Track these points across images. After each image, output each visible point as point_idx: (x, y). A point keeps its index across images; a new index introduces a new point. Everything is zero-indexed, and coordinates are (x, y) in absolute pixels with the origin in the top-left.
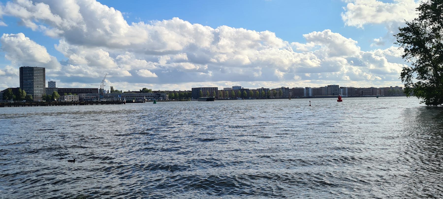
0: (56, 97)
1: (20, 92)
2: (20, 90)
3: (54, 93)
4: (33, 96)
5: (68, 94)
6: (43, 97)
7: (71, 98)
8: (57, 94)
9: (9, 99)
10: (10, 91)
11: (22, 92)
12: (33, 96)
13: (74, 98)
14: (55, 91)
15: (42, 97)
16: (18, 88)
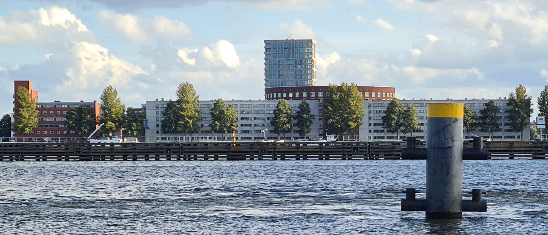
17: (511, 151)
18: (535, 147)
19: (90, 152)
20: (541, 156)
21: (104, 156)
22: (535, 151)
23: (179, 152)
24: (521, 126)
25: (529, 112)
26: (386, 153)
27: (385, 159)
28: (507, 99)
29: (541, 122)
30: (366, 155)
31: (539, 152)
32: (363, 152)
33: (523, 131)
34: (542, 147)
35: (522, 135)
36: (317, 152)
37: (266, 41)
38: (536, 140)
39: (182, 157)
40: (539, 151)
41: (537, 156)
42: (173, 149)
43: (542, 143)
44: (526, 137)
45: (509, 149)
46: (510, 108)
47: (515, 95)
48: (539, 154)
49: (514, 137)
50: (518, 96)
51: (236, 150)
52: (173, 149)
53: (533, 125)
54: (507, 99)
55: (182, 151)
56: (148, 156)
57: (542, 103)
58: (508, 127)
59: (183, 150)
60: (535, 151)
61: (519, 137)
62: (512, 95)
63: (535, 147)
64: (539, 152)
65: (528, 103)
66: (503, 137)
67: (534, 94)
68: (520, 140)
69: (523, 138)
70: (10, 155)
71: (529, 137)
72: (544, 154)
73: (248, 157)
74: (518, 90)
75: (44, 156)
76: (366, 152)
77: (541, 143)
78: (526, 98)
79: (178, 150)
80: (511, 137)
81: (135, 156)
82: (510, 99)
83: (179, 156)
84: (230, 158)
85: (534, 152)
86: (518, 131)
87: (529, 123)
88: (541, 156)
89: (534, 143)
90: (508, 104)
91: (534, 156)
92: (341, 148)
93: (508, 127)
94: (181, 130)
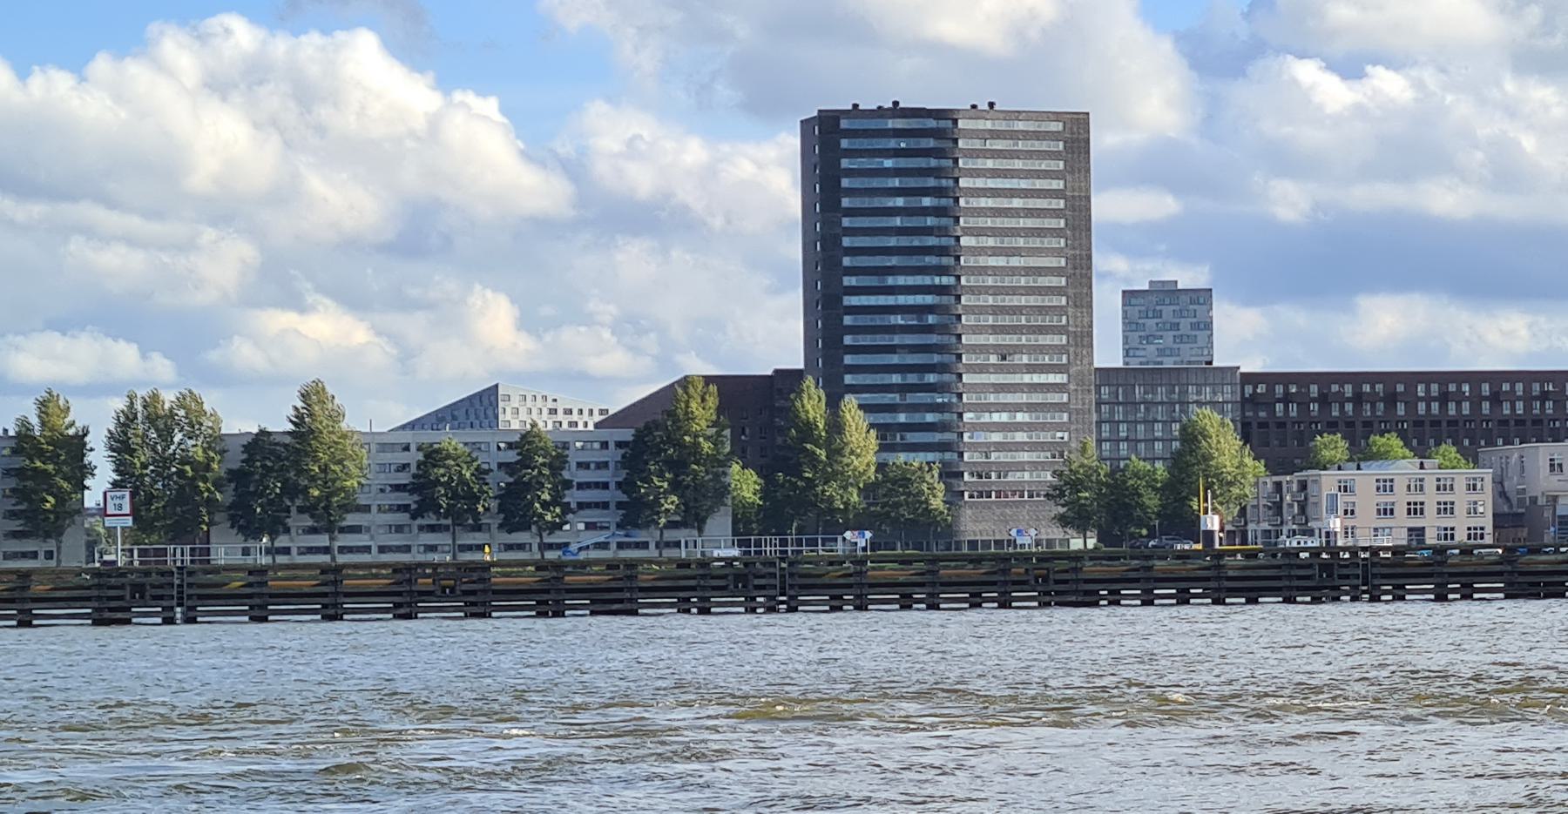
0: (1220, 484)
1: (807, 429)
2: (812, 404)
3: (1191, 436)
4: (950, 474)
5: (1361, 454)
6: (1074, 497)
7: (1401, 498)
8: (1226, 447)
9: (693, 517)
10: (703, 413)
11: (836, 425)
12: (950, 474)
13: (1431, 498)
14: (1209, 419)
15: (1055, 494)
16: (786, 381)
17: (24, 600)
18: (99, 586)
19: (336, 594)
20: (119, 615)
21: (910, 596)
22: (99, 598)
23: (1357, 577)
24: (57, 518)
25: (80, 472)
26: (472, 599)
27: (593, 613)
28: (11, 433)
29: (120, 507)
30: (773, 598)
31: (113, 604)
32: (161, 597)
33: (64, 538)
34: (122, 587)
35: (59, 548)
36: (1137, 580)
37: (1124, 292)
38: (105, 563)
39: (782, 602)
40: (1300, 578)
41: (107, 615)
42: (153, 587)
43: (123, 575)
44: (72, 555)
45: (16, 594)
46: (21, 462)
47: (34, 421)
48: (111, 610)
49: (34, 555)
50: (43, 424)
51: (954, 579)
52: (153, 587)
53: (93, 515)
54: (11, 433)
55: (783, 582)
56: (1402, 587)
57: (121, 445)
58: (15, 525)
59: (788, 581)
60: (99, 598)
61: (49, 555)
62: (24, 423)
63: (99, 586)
64: (113, 604)
65: (76, 445)
66: (374, 550)
67: (95, 421)
68: (53, 563)
69: (63, 558)
70: (1464, 580)
71: (83, 559)
72: (128, 609)
73: (1386, 592)
74: (43, 406)
75: (701, 599)
76: (1357, 577)
77: (121, 573)
78: (71, 432)
79: (772, 581)
80: (24, 555)
81: (263, 607)
82: (19, 434)
83: (773, 598)
84: (1514, 593)
85: (929, 590)
86: (47, 535)
87: (81, 510)
88: (119, 615)
89: (96, 573)
90: (15, 452)
91: (96, 616)
92: (89, 588)
93: (15, 525)
94: (488, 522)
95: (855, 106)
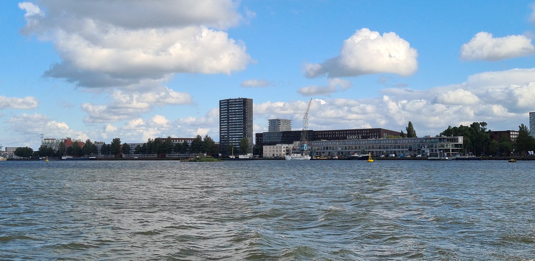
95: (236, 111)
